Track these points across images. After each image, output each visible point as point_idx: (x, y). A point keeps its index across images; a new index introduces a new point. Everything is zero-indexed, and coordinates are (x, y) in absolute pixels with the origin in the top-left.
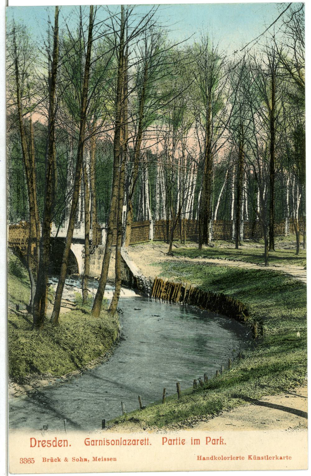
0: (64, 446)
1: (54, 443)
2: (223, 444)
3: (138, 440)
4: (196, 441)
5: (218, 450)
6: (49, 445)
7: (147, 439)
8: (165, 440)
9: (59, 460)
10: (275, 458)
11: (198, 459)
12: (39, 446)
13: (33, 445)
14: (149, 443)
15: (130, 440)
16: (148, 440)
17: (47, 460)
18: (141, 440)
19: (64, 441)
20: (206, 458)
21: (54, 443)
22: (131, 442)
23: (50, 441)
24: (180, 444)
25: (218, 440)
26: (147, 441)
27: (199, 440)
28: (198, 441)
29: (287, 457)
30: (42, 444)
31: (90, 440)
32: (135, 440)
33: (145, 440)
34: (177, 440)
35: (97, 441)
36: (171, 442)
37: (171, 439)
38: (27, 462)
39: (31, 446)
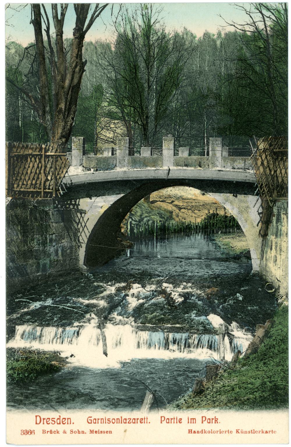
0: (68, 424)
1: (58, 421)
2: (217, 423)
3: (138, 419)
4: (192, 420)
5: (213, 427)
6: (53, 422)
7: (146, 418)
8: (163, 419)
9: (58, 432)
10: (261, 432)
11: (189, 433)
13: (38, 422)
14: (148, 422)
15: (131, 419)
16: (147, 419)
17: (46, 432)
18: (141, 419)
19: (68, 419)
20: (196, 432)
21: (58, 421)
23: (54, 419)
24: (177, 423)
25: (213, 419)
26: (146, 420)
27: (195, 419)
28: (194, 420)
29: (272, 431)
30: (47, 422)
31: (92, 419)
33: (145, 419)
34: (174, 419)
35: (98, 419)
36: (169, 421)
37: (134, 418)
38: (28, 433)
39: (36, 423)
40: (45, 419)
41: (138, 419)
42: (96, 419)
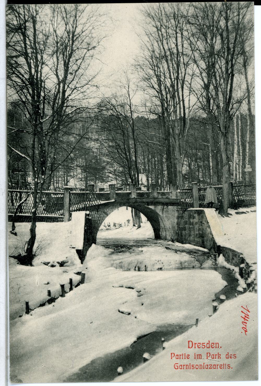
3: (218, 365)
6: (204, 347)
12: (195, 348)
13: (190, 346)
21: (208, 345)
22: (212, 367)
23: (204, 343)
26: (225, 365)
31: (178, 365)
32: (215, 365)
39: (189, 347)
40: (196, 343)
41: (218, 365)
42: (181, 366)
